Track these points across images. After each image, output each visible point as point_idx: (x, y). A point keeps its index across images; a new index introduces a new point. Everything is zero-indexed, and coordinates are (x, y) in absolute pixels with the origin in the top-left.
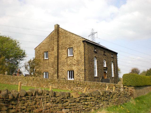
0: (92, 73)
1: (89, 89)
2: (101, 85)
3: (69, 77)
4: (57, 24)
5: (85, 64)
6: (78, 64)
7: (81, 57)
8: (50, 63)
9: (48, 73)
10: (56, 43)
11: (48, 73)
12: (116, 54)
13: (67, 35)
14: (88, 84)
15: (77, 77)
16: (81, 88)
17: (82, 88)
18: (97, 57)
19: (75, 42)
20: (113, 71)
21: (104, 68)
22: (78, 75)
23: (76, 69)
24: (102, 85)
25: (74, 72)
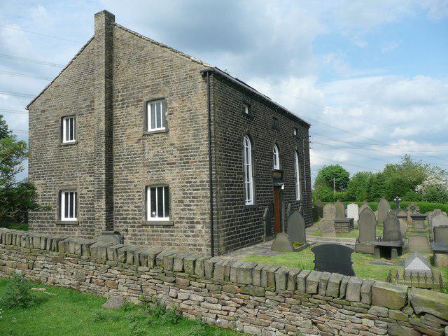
0: (236, 193)
1: (243, 305)
2: (312, 288)
3: (153, 209)
4: (105, 12)
5: (211, 161)
6: (186, 162)
7: (195, 136)
8: (84, 158)
9: (76, 193)
10: (103, 81)
11: (76, 193)
12: (307, 126)
13: (143, 53)
14: (232, 278)
15: (182, 210)
16: (197, 298)
17: (201, 298)
18: (252, 133)
19: (175, 78)
20: (298, 183)
21: (275, 174)
22: (185, 205)
23: (176, 181)
24: (322, 292)
25: (171, 192)
